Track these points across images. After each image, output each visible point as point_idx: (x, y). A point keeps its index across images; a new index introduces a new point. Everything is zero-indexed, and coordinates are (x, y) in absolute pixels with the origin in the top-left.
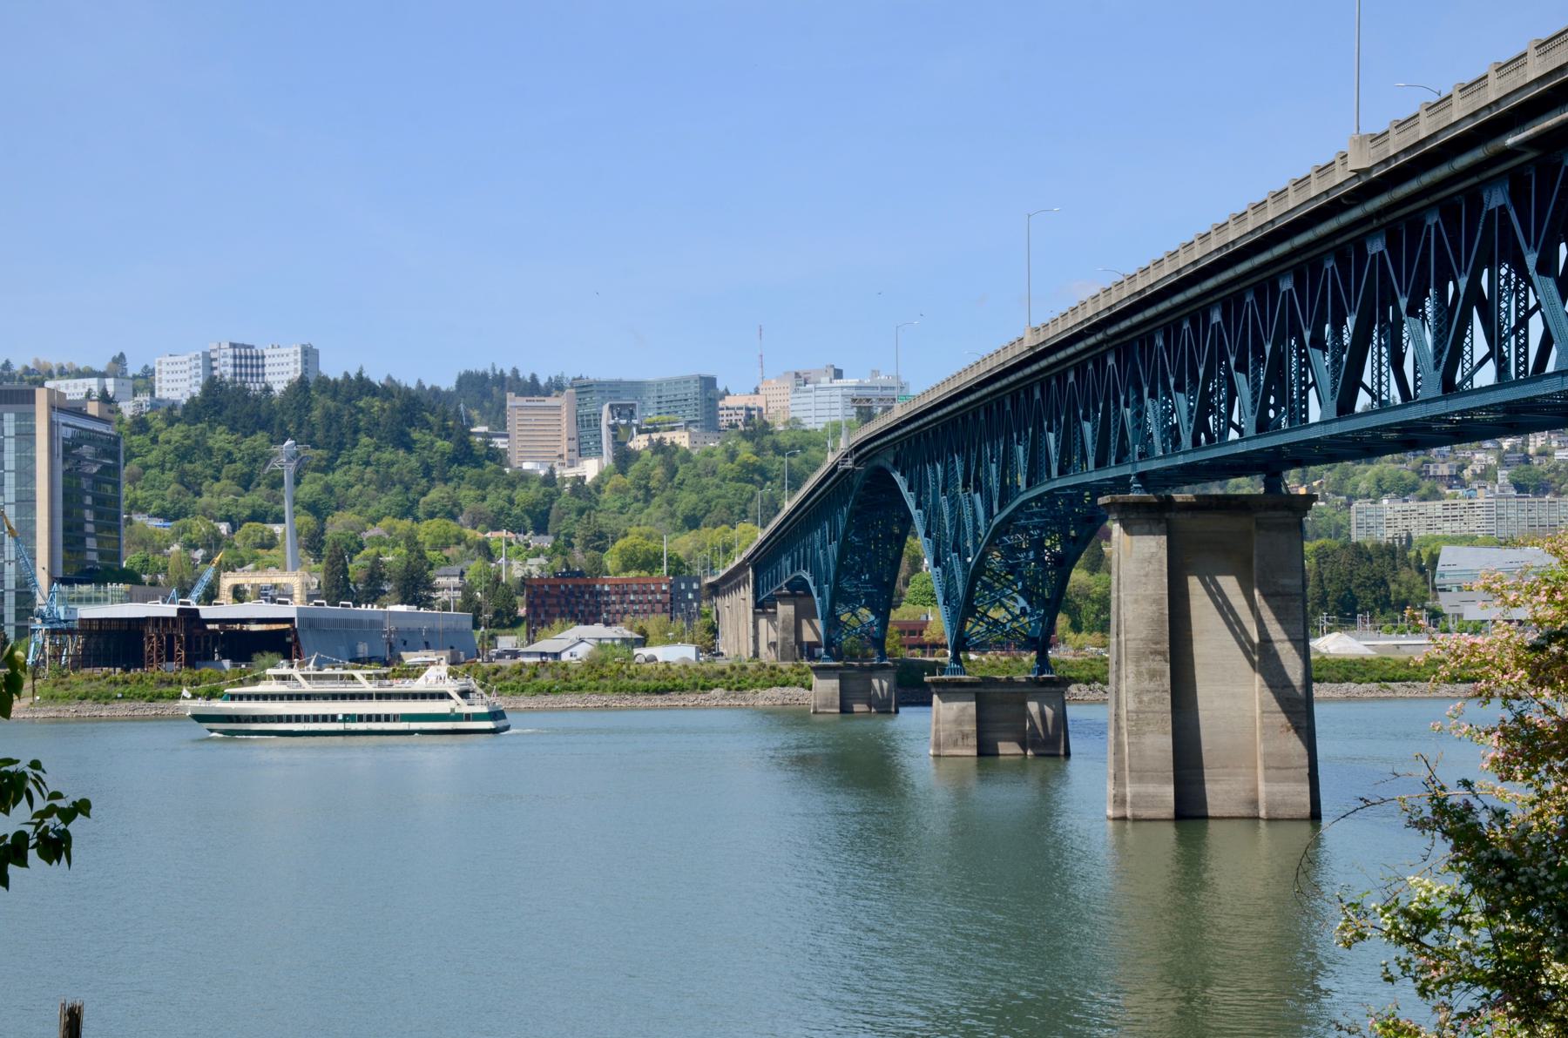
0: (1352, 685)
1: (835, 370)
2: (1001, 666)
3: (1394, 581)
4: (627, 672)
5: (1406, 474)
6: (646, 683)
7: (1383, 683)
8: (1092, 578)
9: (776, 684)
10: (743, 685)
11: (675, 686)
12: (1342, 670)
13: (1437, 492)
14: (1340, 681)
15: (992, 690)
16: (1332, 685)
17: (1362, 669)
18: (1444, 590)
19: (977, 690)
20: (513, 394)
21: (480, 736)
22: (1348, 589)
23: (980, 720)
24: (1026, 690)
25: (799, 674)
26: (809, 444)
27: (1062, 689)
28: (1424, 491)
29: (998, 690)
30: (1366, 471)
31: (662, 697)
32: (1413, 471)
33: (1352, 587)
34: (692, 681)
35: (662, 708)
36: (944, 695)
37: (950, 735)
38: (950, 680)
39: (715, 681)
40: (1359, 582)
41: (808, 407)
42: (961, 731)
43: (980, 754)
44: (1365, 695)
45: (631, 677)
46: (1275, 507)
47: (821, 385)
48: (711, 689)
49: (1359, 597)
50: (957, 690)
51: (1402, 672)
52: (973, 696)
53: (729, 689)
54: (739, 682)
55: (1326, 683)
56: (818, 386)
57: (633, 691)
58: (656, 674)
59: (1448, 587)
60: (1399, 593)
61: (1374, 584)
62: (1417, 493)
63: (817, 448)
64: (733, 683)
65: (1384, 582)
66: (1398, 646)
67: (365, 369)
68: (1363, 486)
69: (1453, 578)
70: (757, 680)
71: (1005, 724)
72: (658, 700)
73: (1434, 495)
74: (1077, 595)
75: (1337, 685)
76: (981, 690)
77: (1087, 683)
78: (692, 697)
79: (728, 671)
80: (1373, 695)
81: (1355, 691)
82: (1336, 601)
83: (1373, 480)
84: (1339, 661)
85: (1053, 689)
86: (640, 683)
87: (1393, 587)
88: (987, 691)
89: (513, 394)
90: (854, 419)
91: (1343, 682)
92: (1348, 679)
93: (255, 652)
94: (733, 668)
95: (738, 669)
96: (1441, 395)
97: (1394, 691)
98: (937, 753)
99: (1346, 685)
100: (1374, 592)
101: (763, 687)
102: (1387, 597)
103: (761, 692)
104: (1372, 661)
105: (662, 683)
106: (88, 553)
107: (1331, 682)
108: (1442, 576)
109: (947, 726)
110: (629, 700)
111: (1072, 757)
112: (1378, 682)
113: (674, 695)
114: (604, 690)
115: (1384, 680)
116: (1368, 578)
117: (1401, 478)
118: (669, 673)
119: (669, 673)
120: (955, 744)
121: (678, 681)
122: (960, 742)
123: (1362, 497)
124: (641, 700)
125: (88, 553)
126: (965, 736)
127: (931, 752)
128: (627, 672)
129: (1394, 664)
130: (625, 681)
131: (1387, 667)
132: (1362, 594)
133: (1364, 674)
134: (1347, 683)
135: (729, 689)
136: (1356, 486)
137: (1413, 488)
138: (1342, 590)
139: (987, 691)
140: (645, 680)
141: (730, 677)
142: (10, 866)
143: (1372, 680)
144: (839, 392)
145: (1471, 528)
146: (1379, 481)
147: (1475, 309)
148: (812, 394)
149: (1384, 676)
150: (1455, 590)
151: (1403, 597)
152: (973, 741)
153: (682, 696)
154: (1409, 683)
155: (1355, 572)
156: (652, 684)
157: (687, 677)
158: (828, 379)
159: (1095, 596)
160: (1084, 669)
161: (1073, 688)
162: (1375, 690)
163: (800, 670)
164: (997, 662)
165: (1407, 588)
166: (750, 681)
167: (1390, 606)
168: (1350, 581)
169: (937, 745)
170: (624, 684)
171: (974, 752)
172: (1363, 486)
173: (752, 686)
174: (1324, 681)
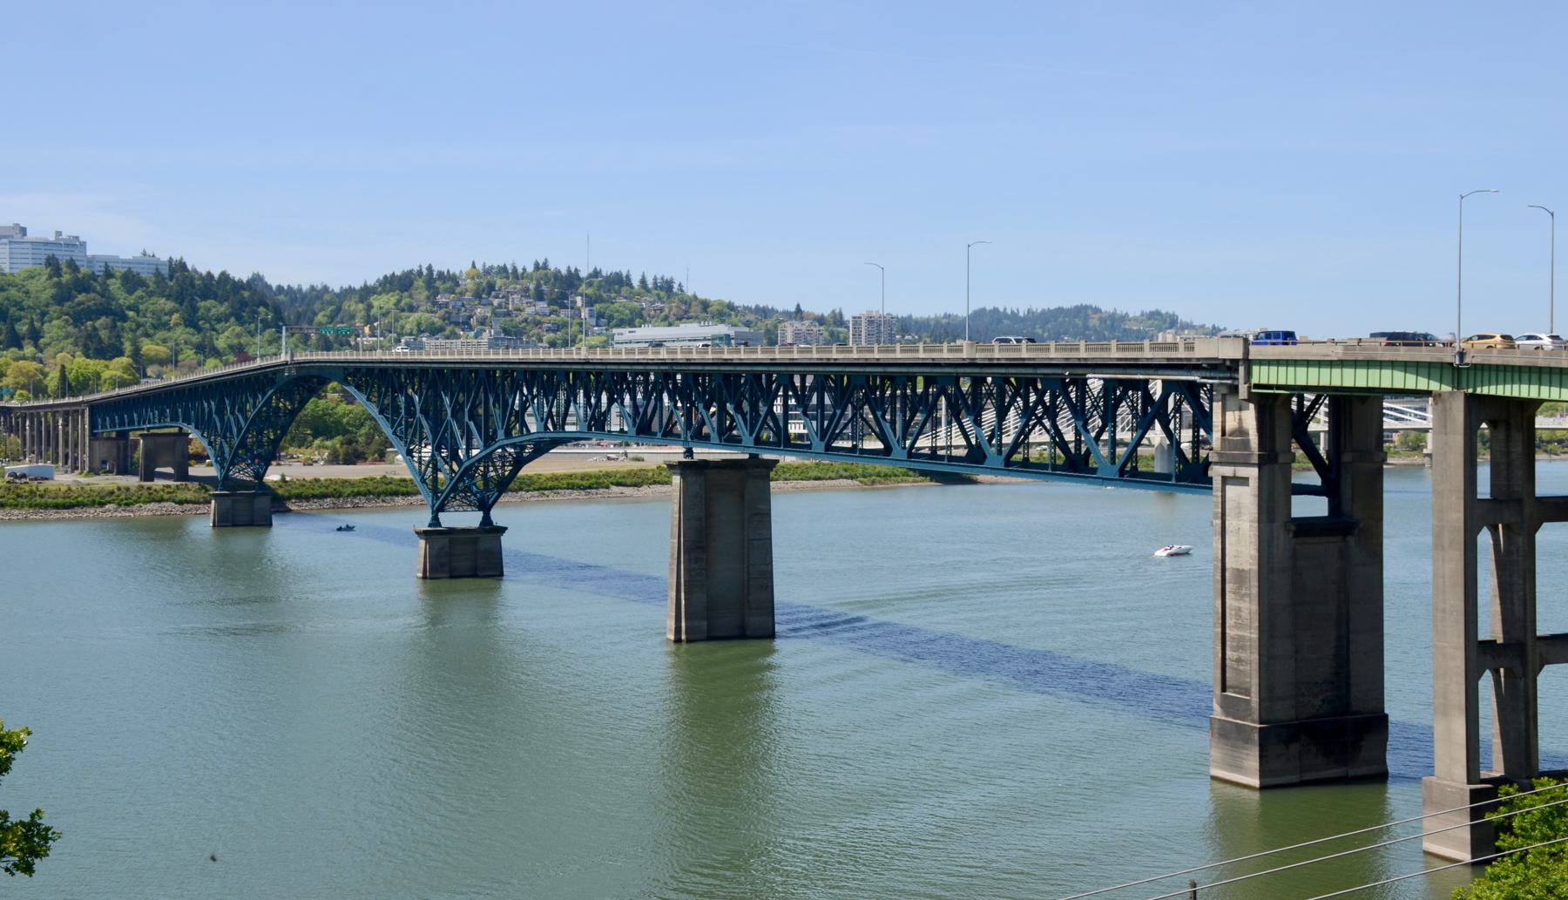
0: (524, 493)
1: (21, 227)
4: (38, 493)
5: (436, 320)
6: (55, 501)
9: (154, 501)
10: (129, 501)
11: (78, 502)
13: (456, 334)
17: (528, 482)
20: (1498, 642)
21: (1227, 551)
25: (169, 493)
26: (9, 285)
28: (447, 332)
30: (409, 317)
31: (69, 510)
32: (440, 318)
34: (90, 499)
35: (70, 520)
39: (108, 499)
41: (27, 261)
45: (42, 496)
46: (758, 467)
47: (14, 240)
48: (105, 504)
51: (550, 484)
53: (119, 505)
54: (126, 499)
56: (11, 240)
57: (46, 506)
58: (61, 494)
62: (444, 333)
63: (15, 289)
64: (122, 500)
67: (631, 273)
68: (408, 327)
70: (139, 498)
72: (66, 514)
73: (454, 335)
76: (452, 536)
77: (365, 495)
78: (92, 510)
79: (116, 491)
83: (415, 323)
86: (50, 501)
89: (1498, 642)
90: (43, 266)
92: (521, 489)
94: (119, 489)
95: (123, 490)
96: (906, 459)
97: (548, 496)
99: (520, 493)
101: (145, 502)
103: (144, 506)
105: (67, 500)
110: (42, 514)
113: (76, 509)
114: (22, 507)
117: (433, 323)
118: (72, 494)
119: (72, 494)
121: (80, 499)
123: (407, 334)
124: (53, 514)
128: (38, 493)
130: (38, 500)
133: (529, 486)
135: (119, 505)
136: (403, 327)
137: (441, 330)
140: (54, 498)
141: (118, 496)
142: (1485, 527)
143: (535, 490)
144: (30, 246)
146: (419, 324)
147: (826, 394)
148: (8, 247)
149: (542, 486)
153: (84, 509)
154: (555, 491)
156: (60, 501)
157: (86, 495)
158: (19, 235)
163: (169, 490)
164: (304, 483)
166: (134, 498)
170: (38, 502)
172: (408, 327)
173: (136, 502)
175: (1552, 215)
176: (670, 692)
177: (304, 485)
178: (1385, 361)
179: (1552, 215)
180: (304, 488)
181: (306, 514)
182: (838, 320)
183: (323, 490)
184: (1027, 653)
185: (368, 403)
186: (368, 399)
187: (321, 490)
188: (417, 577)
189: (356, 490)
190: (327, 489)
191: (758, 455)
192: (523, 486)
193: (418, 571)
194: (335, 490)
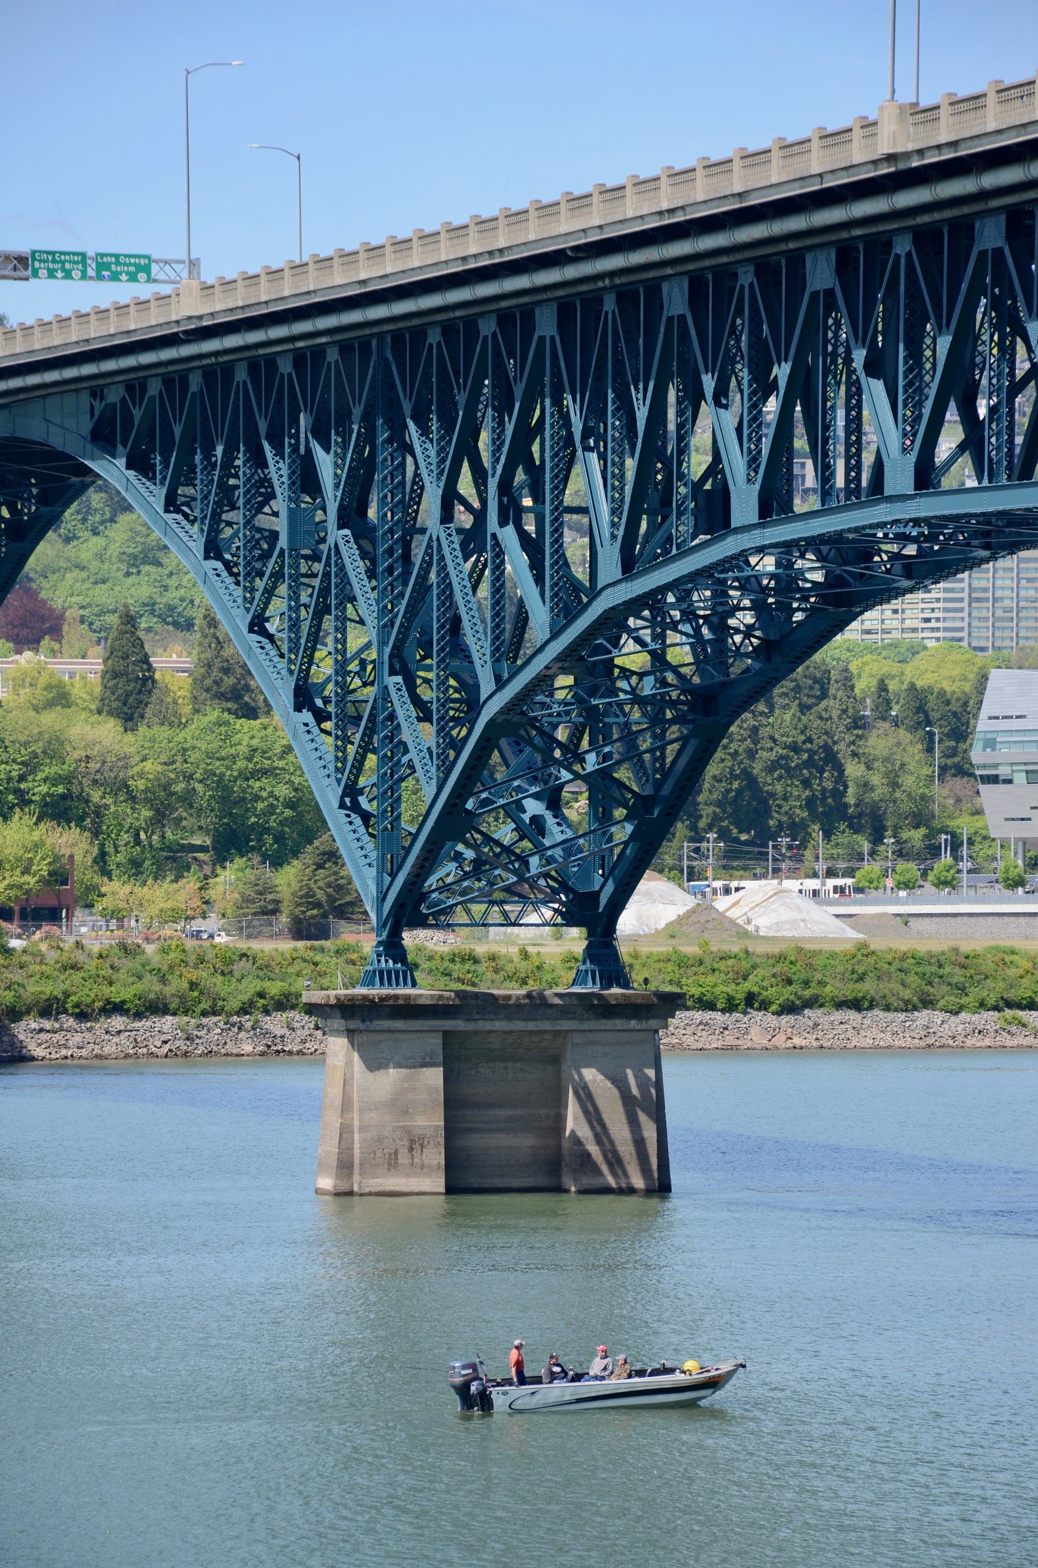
0: (938, 1016)
2: (91, 965)
3: (854, 754)
7: (1009, 1013)
8: (129, 737)
12: (912, 979)
14: (908, 1007)
15: (487, 1026)
16: (890, 1016)
17: (958, 976)
18: (994, 780)
19: (448, 1024)
22: (747, 776)
23: (453, 1103)
24: (565, 1025)
27: (653, 1023)
29: (499, 1025)
33: (757, 768)
36: (365, 1037)
37: (380, 1140)
38: (382, 999)
40: (773, 756)
42: (408, 1130)
43: (452, 1189)
44: (969, 1042)
49: (772, 795)
50: (399, 1024)
52: (436, 1042)
55: (876, 1012)
59: (1003, 771)
60: (866, 786)
61: (809, 764)
65: (831, 759)
66: (906, 919)
69: (1016, 749)
71: (509, 1112)
74: (95, 782)
75: (902, 1016)
76: (459, 1025)
80: (988, 1042)
81: (946, 1030)
82: (719, 804)
84: (903, 958)
85: (633, 1024)
87: (853, 770)
88: (471, 1026)
91: (915, 1008)
92: (927, 1003)
93: (590, 935)
98: (344, 1187)
99: (923, 1016)
100: (806, 783)
102: (839, 794)
104: (977, 956)
106: (692, 661)
107: (887, 1008)
108: (990, 744)
109: (373, 1116)
111: (676, 1201)
112: (996, 1008)
115: (1010, 1005)
116: (795, 748)
120: (392, 1163)
122: (404, 1158)
125: (692, 661)
126: (415, 1143)
127: (326, 1183)
129: (1029, 965)
131: (1012, 972)
132: (779, 788)
134: (925, 1012)
138: (734, 777)
139: (471, 1026)
145: (908, 623)
149: (1012, 995)
150: (1020, 778)
151: (876, 796)
152: (436, 1156)
155: (764, 732)
159: (141, 784)
160: (299, 974)
161: (681, 1018)
162: (991, 1028)
164: (80, 957)
165: (886, 775)
167: (844, 817)
168: (751, 754)
169: (345, 1166)
171: (438, 1183)
174: (871, 1007)
175: (299, 158)
176: (70, 828)
177: (75, 967)
178: (217, 312)
179: (299, 158)
180: (77, 977)
181: (66, 1066)
182: (83, 255)
183: (151, 987)
184: (889, 957)
185: (169, 517)
186: (171, 504)
187: (139, 987)
188: (318, 1191)
189: (274, 988)
190: (163, 980)
191: (275, 498)
192: (939, 991)
193: (321, 1168)
194: (193, 985)
